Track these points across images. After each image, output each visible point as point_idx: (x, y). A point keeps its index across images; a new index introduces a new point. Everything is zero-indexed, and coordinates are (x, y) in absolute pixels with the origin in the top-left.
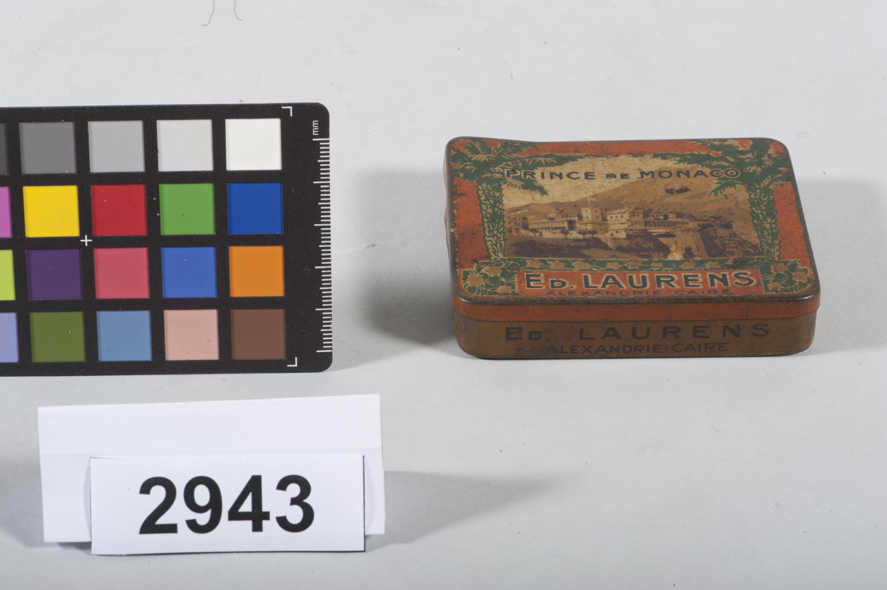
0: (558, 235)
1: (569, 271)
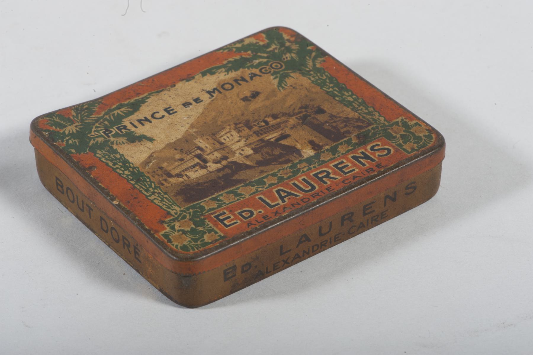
0: (202, 172)
1: (242, 199)
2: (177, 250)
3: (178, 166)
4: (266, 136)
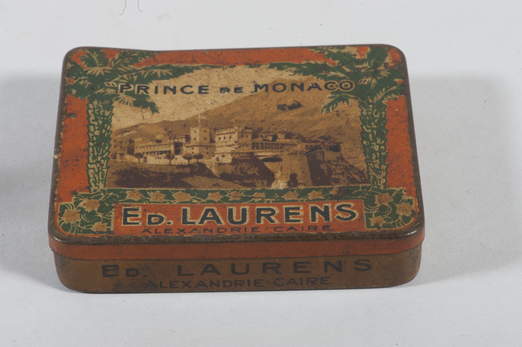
0: (163, 161)
4: (259, 152)
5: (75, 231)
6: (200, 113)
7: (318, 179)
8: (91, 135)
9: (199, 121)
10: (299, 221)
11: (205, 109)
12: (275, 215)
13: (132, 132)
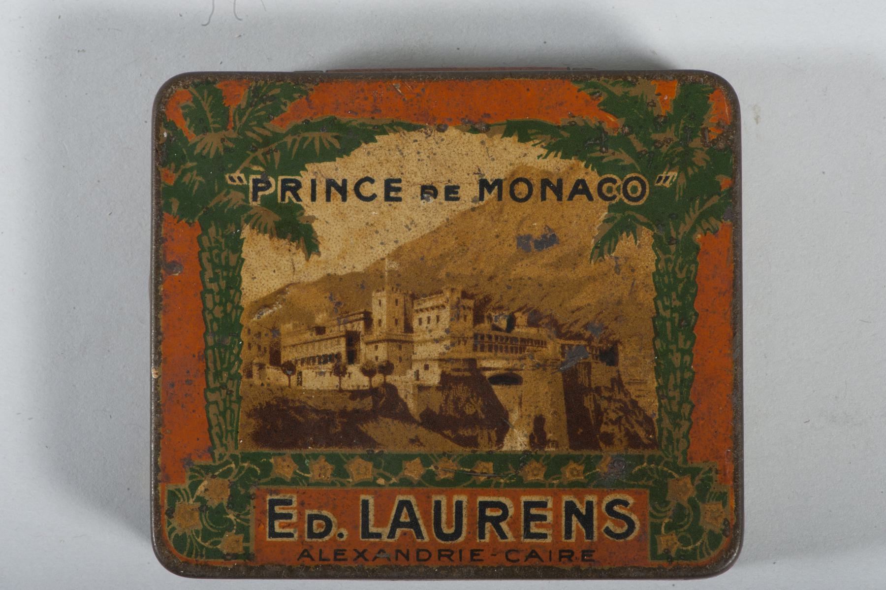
0: (329, 382)
2: (168, 538)
3: (306, 343)
4: (485, 359)
5: (194, 552)
6: (387, 252)
7: (579, 433)
8: (209, 317)
9: (386, 274)
10: (544, 536)
11: (396, 242)
12: (508, 519)
13: (275, 308)
